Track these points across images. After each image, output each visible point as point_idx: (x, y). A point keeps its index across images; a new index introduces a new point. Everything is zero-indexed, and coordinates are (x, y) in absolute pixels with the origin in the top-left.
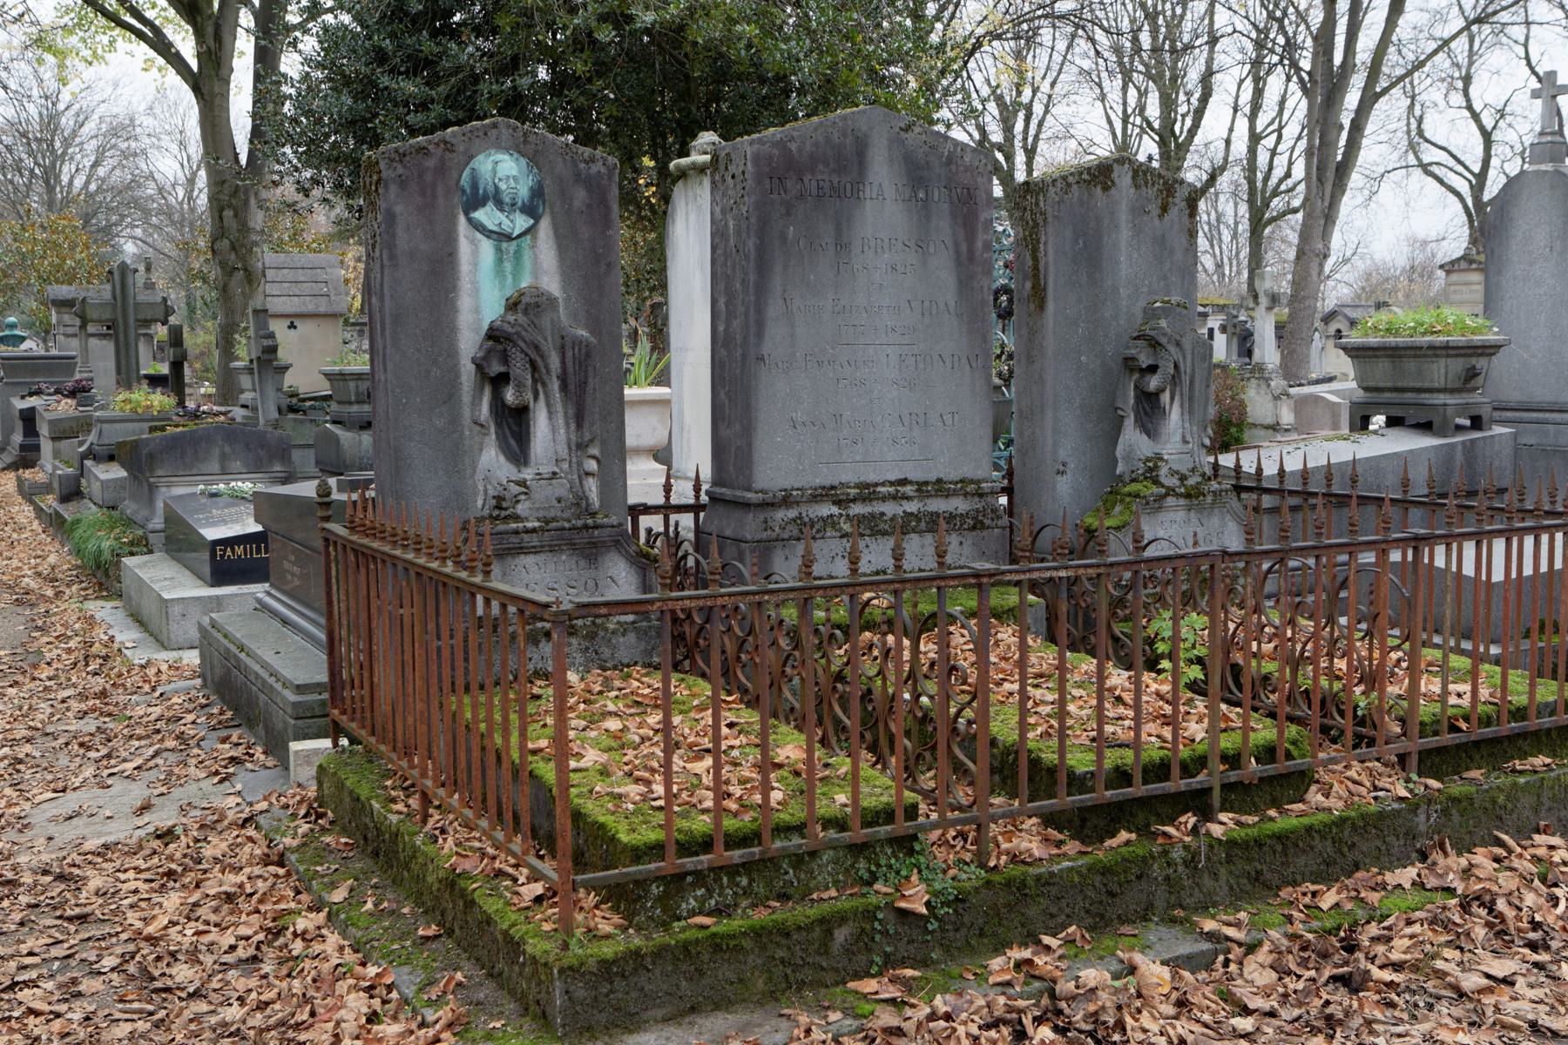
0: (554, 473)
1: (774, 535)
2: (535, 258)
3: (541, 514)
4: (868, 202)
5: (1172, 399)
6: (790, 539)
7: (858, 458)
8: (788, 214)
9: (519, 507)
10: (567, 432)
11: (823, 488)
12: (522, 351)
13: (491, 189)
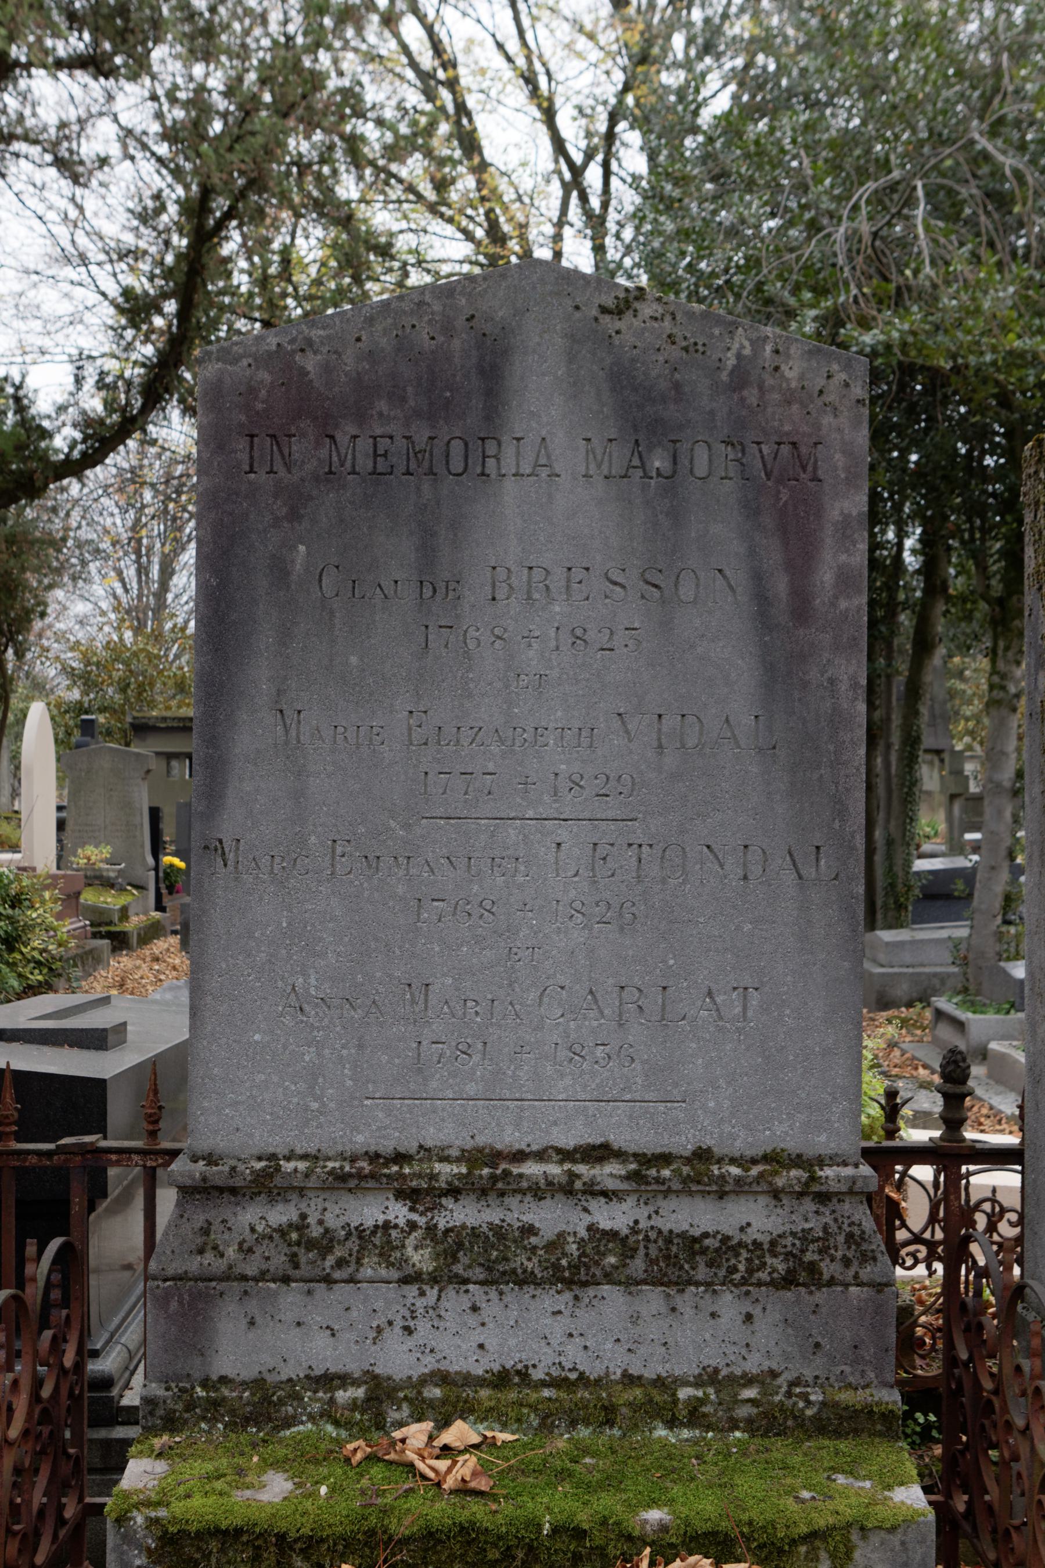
1: (219, 1266)
4: (509, 483)
6: (262, 1276)
7: (471, 1089)
8: (294, 515)
11: (374, 1157)
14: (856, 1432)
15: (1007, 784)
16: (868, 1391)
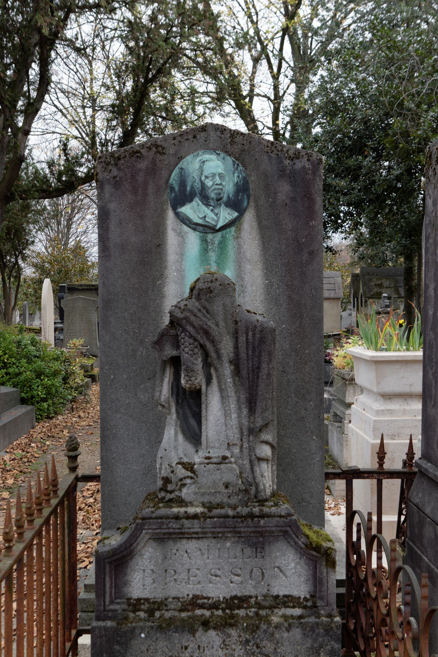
0: (225, 458)
2: (239, 247)
3: (206, 499)
9: (184, 490)
10: (239, 416)
12: (191, 336)
13: (198, 185)
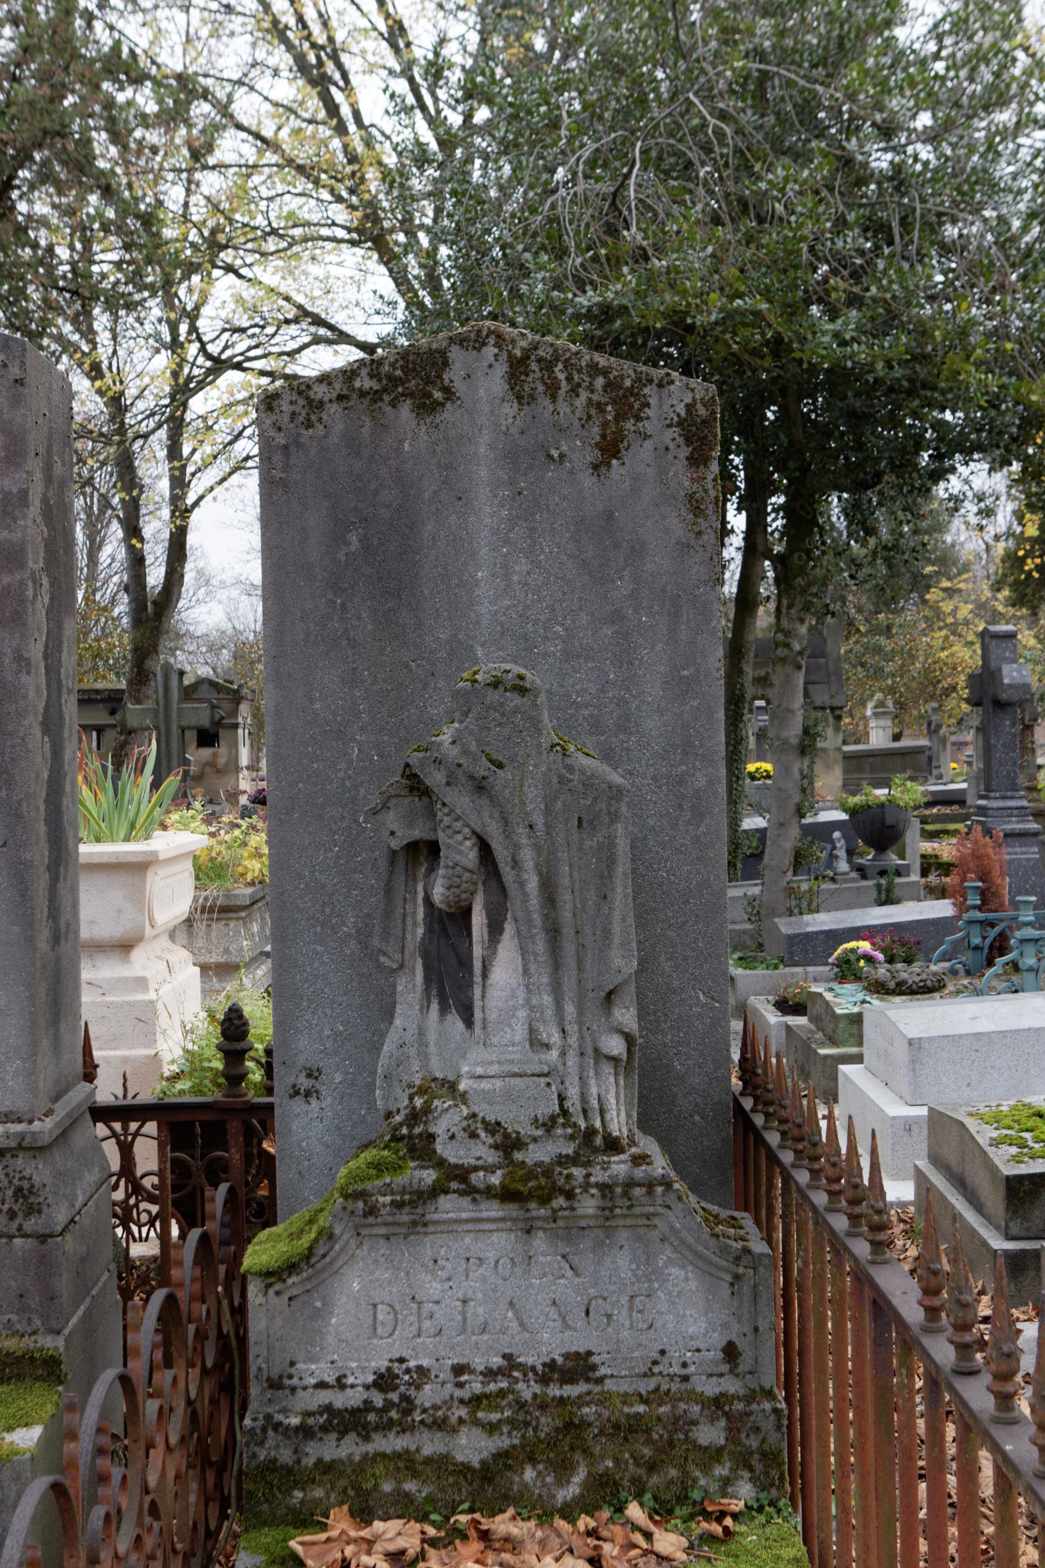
5: (495, 930)
14: (20, 1377)
15: (794, 741)
16: (33, 1338)
